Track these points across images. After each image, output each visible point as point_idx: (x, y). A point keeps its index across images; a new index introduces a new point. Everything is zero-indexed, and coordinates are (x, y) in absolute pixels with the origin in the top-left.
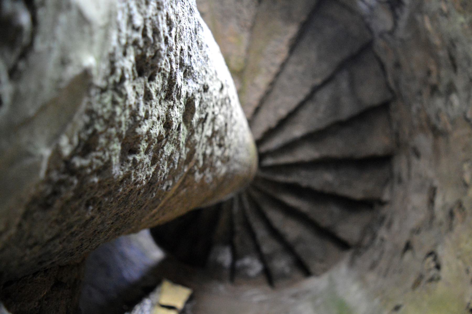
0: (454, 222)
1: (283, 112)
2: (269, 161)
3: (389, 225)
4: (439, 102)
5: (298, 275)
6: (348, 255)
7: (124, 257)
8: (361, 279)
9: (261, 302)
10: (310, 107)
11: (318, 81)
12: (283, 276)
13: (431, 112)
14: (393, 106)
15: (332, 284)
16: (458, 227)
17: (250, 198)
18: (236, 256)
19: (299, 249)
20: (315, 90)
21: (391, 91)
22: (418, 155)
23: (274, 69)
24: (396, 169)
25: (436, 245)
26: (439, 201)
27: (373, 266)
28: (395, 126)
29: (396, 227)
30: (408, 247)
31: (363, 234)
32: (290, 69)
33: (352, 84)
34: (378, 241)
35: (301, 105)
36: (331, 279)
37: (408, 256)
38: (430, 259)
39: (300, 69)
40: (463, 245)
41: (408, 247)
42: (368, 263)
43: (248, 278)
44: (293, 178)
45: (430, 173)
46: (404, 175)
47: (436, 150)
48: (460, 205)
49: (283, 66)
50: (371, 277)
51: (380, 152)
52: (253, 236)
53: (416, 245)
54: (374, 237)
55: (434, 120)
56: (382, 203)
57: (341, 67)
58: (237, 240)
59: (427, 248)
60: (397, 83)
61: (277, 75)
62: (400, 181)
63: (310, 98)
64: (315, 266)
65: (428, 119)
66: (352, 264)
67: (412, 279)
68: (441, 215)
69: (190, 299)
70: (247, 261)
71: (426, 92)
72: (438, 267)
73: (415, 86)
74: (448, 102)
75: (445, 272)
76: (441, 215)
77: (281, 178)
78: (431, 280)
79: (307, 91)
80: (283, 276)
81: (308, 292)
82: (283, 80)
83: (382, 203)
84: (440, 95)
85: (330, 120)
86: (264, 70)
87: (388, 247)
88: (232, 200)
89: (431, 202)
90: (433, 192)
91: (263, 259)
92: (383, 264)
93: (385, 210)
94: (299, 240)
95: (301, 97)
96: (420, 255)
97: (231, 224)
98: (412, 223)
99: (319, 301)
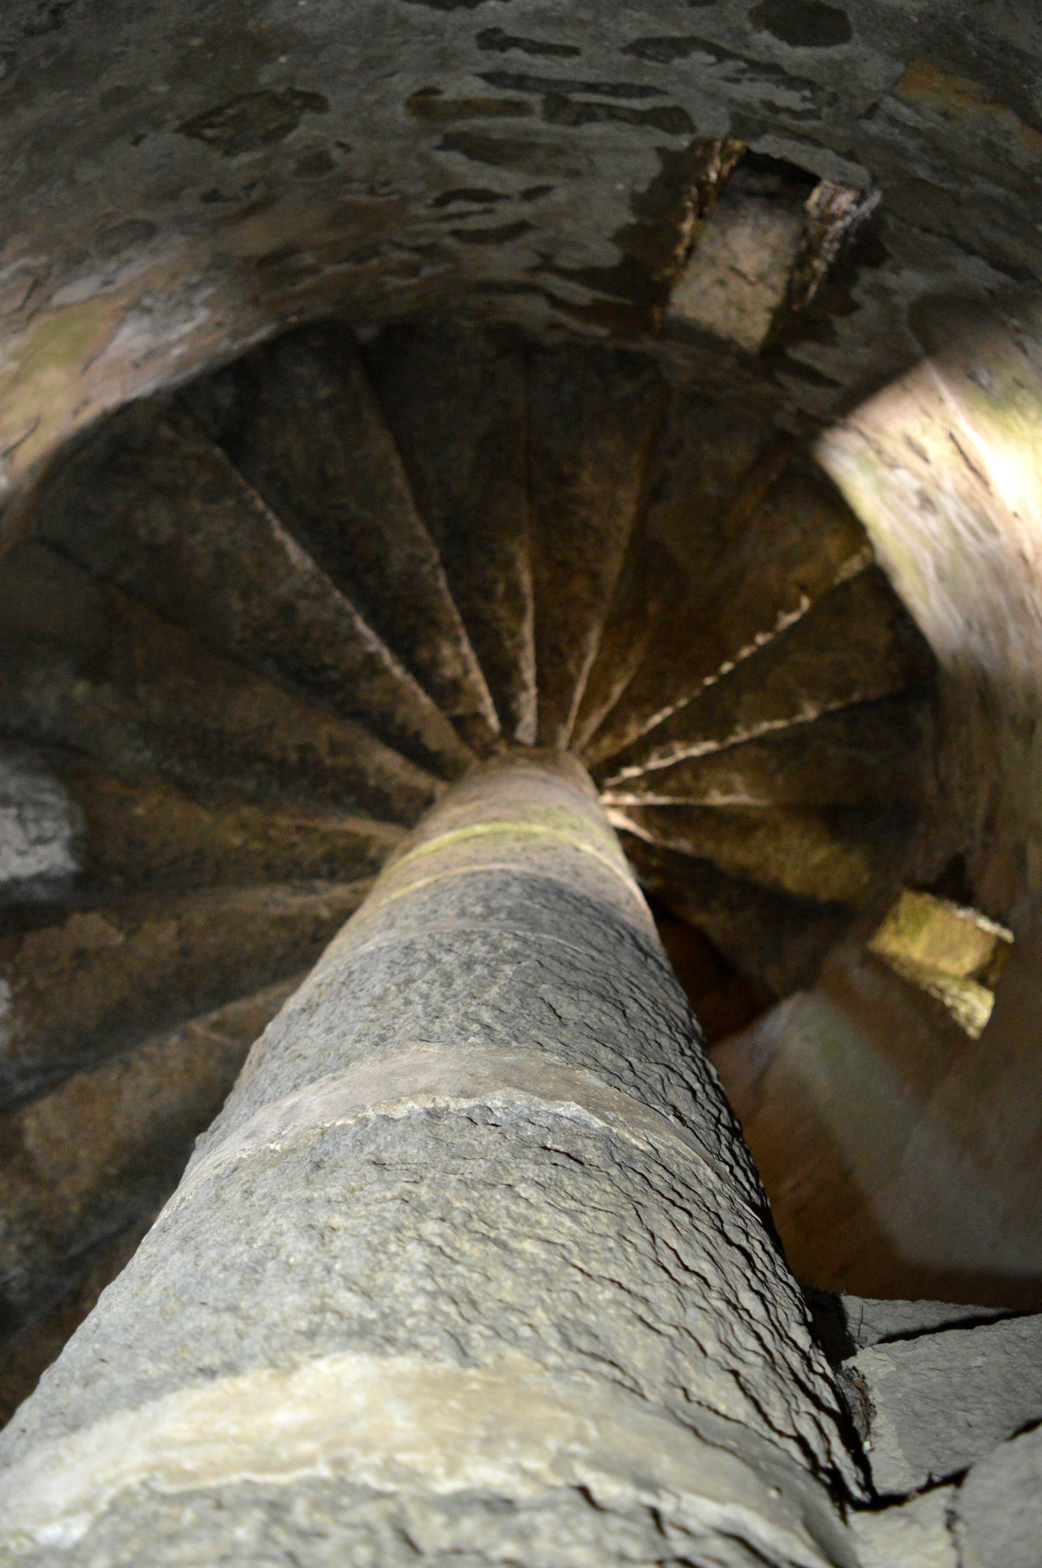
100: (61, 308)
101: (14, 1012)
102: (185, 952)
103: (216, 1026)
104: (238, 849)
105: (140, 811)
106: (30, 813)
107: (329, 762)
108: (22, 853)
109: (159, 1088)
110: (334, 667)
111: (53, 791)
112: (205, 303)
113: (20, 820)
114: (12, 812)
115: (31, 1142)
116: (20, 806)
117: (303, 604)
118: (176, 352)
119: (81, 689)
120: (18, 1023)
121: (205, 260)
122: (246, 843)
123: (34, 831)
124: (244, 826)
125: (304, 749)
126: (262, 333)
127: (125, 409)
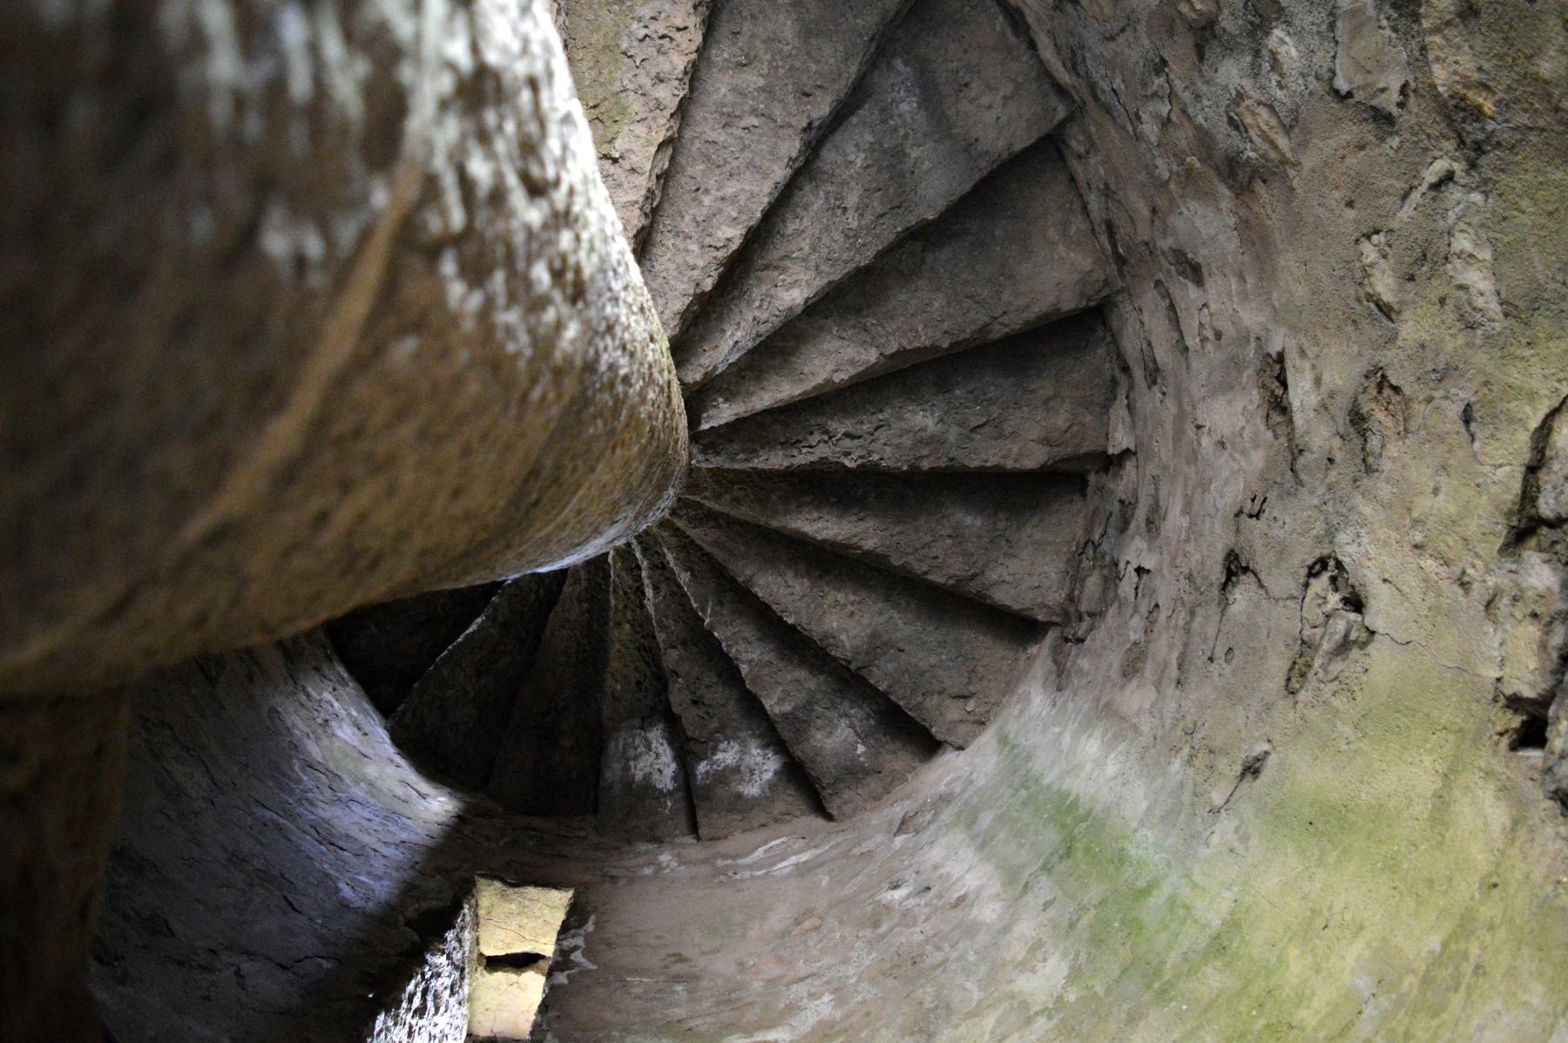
0: (1374, 443)
1: (731, 234)
2: (723, 413)
3: (1152, 524)
4: (1232, 72)
5: (897, 758)
6: (1041, 651)
7: (328, 837)
8: (1106, 711)
9: (802, 870)
10: (814, 200)
11: (822, 108)
12: (854, 773)
13: (1209, 114)
14: (1076, 143)
15: (1013, 753)
16: (1393, 453)
17: (687, 547)
18: (686, 753)
19: (880, 677)
20: (818, 139)
21: (1061, 91)
22: (1195, 273)
23: (669, 95)
24: (1131, 345)
25: (1330, 534)
26: (1301, 393)
27: (1132, 668)
28: (1094, 202)
29: (1175, 520)
30: (1235, 567)
31: (1075, 576)
32: (720, 87)
33: (930, 97)
34: (1126, 587)
35: (783, 201)
36: (1003, 740)
37: (1242, 594)
38: (1321, 584)
39: (753, 79)
40: (1423, 504)
41: (1235, 567)
42: (1115, 660)
43: (741, 806)
44: (813, 451)
45: (1252, 317)
46: (1164, 355)
47: (1253, 235)
48: (1381, 381)
49: (694, 75)
50: (1136, 698)
51: (1069, 303)
52: (729, 672)
53: (1262, 560)
54: (1112, 575)
55: (1225, 139)
56: (1111, 463)
57: (881, 50)
58: (678, 698)
59: (1306, 554)
60: (1074, 63)
61: (683, 111)
62: (1154, 374)
63: (804, 171)
64: (944, 716)
65: (1204, 140)
66: (1060, 677)
67: (1278, 664)
68: (1319, 436)
69: (574, 919)
70: (727, 755)
71: (1179, 51)
72: (1355, 603)
73: (1135, 49)
74: (1262, 60)
75: (1382, 610)
76: (1319, 436)
77: (774, 460)
78: (1344, 646)
79: (792, 146)
80: (854, 773)
81: (945, 799)
82: (705, 126)
83: (1111, 463)
84: (1230, 49)
85: (888, 232)
86: (636, 105)
87: (1166, 589)
88: (629, 545)
89: (1279, 406)
90: (1276, 371)
91: (774, 736)
92: (1164, 648)
93: (1126, 481)
94: (877, 645)
95: (780, 173)
96: (1282, 582)
97: (649, 652)
98: (1229, 492)
99: (986, 819)
100: (324, 758)
101: (736, 738)
102: (684, 643)
103: (704, 611)
104: (632, 626)
105: (619, 687)
106: (631, 753)
107: (584, 584)
108: (658, 756)
109: (745, 639)
110: (537, 593)
111: (617, 740)
112: (320, 694)
113: (636, 758)
114: (632, 764)
115: (787, 708)
116: (628, 760)
117: (500, 619)
118: (354, 713)
119: (566, 743)
120: (741, 735)
121: (290, 688)
122: (628, 622)
123: (641, 749)
124: (618, 624)
125: (580, 600)
126: (341, 670)
127: (396, 741)
